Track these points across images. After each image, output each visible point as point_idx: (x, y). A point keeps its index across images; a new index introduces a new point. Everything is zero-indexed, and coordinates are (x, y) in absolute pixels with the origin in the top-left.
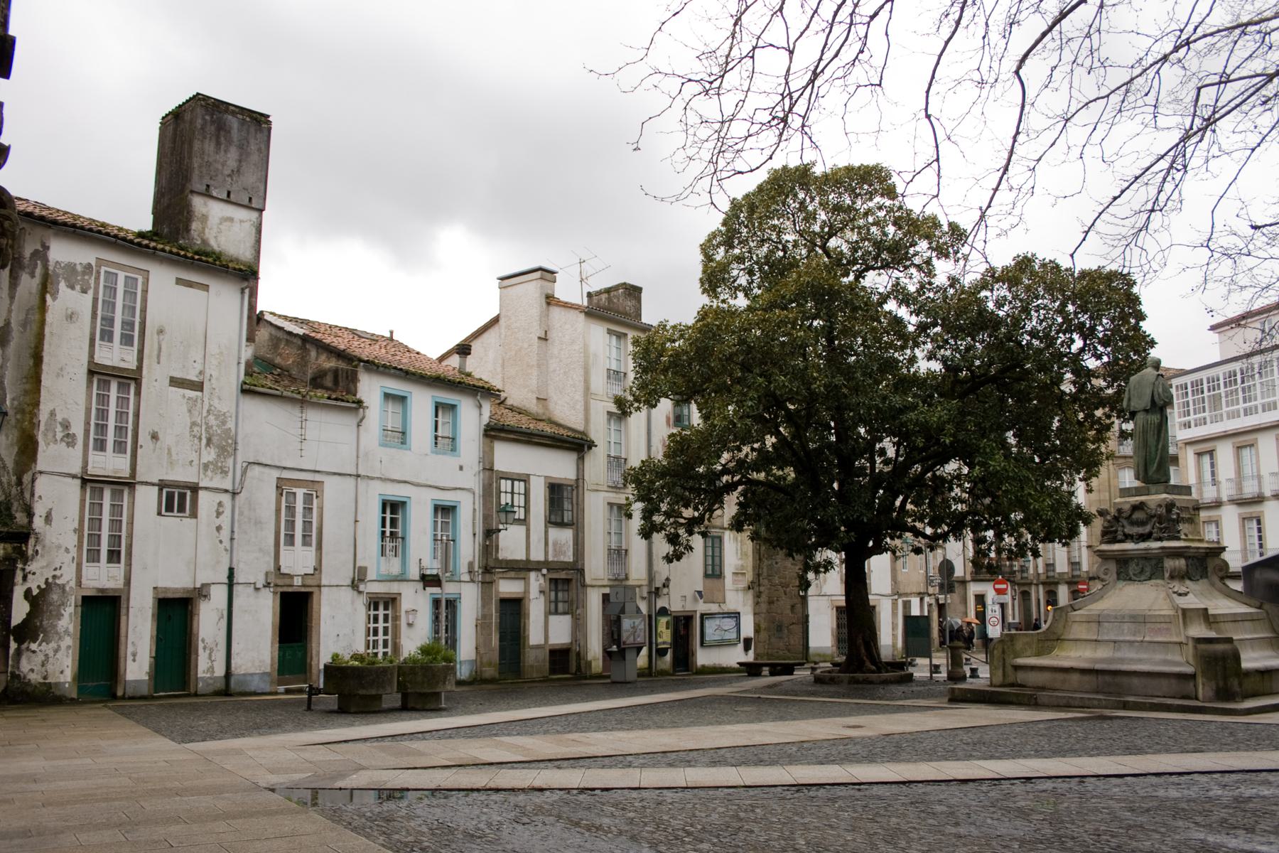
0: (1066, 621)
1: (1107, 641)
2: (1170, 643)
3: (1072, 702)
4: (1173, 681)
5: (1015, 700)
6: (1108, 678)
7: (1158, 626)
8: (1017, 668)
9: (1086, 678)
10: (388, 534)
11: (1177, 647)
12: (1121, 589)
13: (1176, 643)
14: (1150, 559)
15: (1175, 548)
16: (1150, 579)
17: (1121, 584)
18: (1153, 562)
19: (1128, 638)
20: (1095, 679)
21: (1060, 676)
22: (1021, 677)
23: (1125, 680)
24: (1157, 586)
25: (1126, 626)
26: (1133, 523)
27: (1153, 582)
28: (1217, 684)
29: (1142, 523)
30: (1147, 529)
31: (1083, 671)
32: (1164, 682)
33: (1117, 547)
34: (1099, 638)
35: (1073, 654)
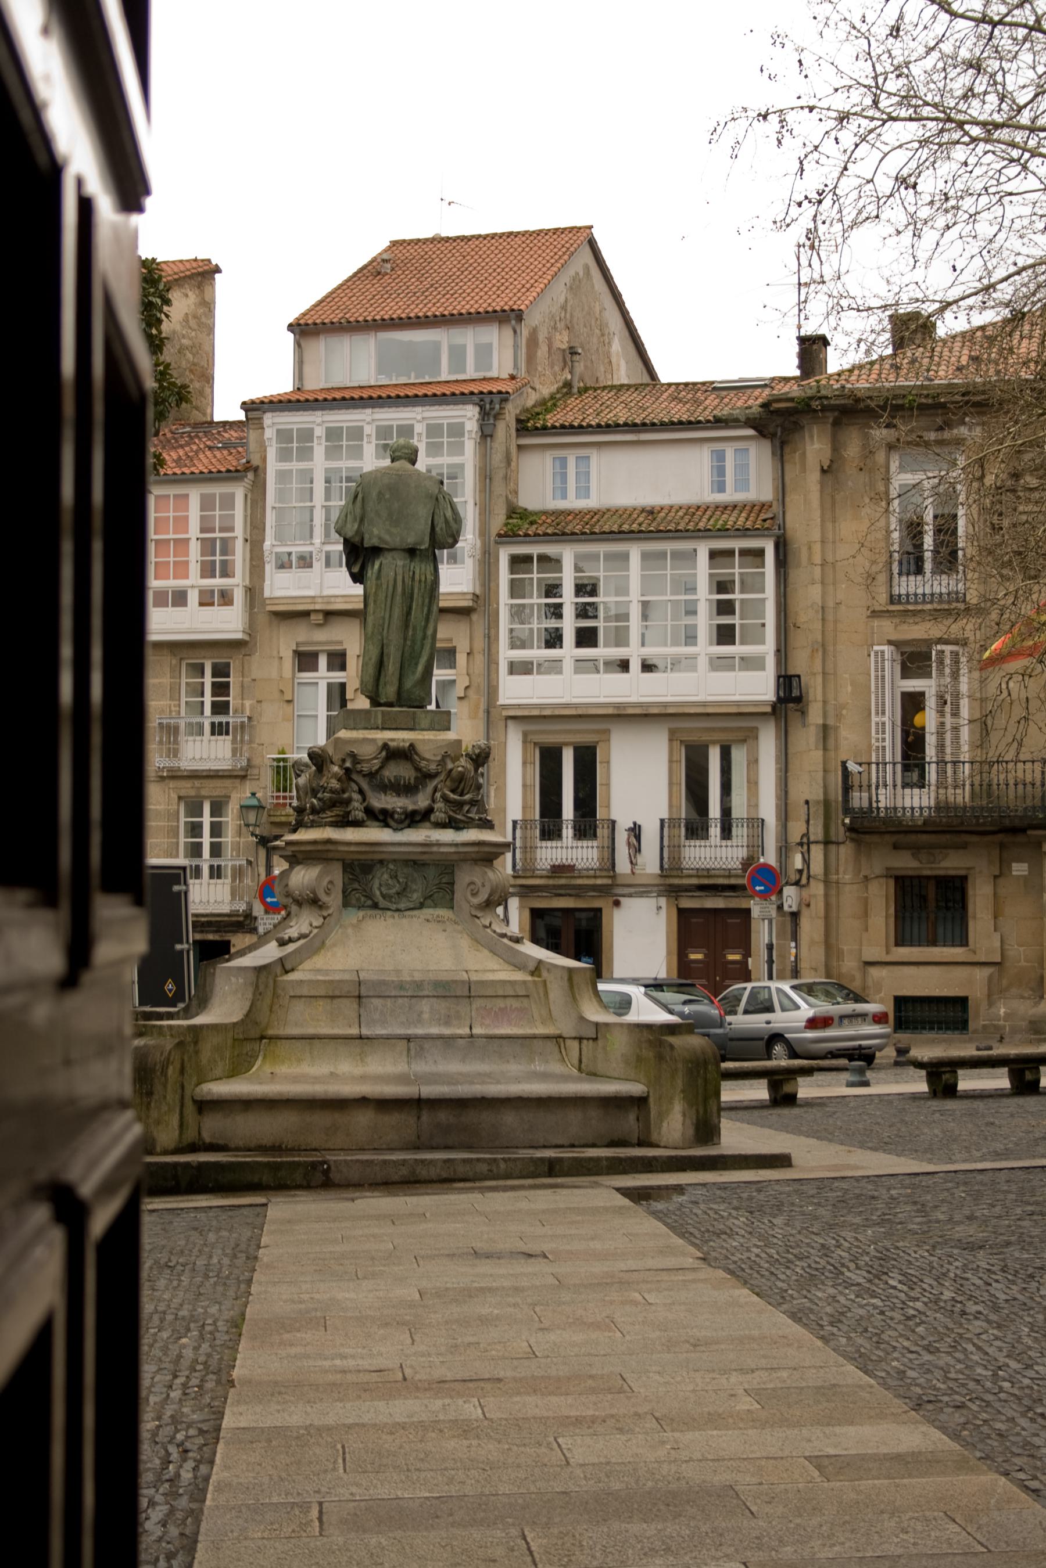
0: (275, 995)
1: (388, 1038)
2: (534, 1037)
3: (423, 1173)
4: (594, 1113)
5: (266, 1178)
6: (443, 1116)
7: (500, 1003)
8: (204, 1106)
9: (393, 1119)
10: (948, 726)
11: (551, 1045)
12: (357, 927)
13: (547, 1037)
14: (424, 864)
15: (315, 842)
16: (421, 906)
17: (353, 916)
18: (431, 873)
19: (434, 1030)
20: (412, 1121)
21: (321, 1119)
22: (212, 1126)
23: (486, 1118)
24: (439, 921)
25: (425, 1006)
26: (385, 787)
27: (427, 912)
28: (697, 1111)
29: (408, 789)
30: (422, 801)
31: (384, 1104)
32: (574, 1118)
33: (350, 835)
34: (365, 1032)
35: (307, 1069)
